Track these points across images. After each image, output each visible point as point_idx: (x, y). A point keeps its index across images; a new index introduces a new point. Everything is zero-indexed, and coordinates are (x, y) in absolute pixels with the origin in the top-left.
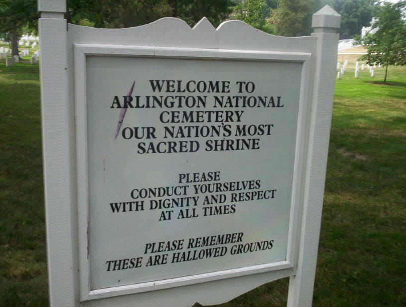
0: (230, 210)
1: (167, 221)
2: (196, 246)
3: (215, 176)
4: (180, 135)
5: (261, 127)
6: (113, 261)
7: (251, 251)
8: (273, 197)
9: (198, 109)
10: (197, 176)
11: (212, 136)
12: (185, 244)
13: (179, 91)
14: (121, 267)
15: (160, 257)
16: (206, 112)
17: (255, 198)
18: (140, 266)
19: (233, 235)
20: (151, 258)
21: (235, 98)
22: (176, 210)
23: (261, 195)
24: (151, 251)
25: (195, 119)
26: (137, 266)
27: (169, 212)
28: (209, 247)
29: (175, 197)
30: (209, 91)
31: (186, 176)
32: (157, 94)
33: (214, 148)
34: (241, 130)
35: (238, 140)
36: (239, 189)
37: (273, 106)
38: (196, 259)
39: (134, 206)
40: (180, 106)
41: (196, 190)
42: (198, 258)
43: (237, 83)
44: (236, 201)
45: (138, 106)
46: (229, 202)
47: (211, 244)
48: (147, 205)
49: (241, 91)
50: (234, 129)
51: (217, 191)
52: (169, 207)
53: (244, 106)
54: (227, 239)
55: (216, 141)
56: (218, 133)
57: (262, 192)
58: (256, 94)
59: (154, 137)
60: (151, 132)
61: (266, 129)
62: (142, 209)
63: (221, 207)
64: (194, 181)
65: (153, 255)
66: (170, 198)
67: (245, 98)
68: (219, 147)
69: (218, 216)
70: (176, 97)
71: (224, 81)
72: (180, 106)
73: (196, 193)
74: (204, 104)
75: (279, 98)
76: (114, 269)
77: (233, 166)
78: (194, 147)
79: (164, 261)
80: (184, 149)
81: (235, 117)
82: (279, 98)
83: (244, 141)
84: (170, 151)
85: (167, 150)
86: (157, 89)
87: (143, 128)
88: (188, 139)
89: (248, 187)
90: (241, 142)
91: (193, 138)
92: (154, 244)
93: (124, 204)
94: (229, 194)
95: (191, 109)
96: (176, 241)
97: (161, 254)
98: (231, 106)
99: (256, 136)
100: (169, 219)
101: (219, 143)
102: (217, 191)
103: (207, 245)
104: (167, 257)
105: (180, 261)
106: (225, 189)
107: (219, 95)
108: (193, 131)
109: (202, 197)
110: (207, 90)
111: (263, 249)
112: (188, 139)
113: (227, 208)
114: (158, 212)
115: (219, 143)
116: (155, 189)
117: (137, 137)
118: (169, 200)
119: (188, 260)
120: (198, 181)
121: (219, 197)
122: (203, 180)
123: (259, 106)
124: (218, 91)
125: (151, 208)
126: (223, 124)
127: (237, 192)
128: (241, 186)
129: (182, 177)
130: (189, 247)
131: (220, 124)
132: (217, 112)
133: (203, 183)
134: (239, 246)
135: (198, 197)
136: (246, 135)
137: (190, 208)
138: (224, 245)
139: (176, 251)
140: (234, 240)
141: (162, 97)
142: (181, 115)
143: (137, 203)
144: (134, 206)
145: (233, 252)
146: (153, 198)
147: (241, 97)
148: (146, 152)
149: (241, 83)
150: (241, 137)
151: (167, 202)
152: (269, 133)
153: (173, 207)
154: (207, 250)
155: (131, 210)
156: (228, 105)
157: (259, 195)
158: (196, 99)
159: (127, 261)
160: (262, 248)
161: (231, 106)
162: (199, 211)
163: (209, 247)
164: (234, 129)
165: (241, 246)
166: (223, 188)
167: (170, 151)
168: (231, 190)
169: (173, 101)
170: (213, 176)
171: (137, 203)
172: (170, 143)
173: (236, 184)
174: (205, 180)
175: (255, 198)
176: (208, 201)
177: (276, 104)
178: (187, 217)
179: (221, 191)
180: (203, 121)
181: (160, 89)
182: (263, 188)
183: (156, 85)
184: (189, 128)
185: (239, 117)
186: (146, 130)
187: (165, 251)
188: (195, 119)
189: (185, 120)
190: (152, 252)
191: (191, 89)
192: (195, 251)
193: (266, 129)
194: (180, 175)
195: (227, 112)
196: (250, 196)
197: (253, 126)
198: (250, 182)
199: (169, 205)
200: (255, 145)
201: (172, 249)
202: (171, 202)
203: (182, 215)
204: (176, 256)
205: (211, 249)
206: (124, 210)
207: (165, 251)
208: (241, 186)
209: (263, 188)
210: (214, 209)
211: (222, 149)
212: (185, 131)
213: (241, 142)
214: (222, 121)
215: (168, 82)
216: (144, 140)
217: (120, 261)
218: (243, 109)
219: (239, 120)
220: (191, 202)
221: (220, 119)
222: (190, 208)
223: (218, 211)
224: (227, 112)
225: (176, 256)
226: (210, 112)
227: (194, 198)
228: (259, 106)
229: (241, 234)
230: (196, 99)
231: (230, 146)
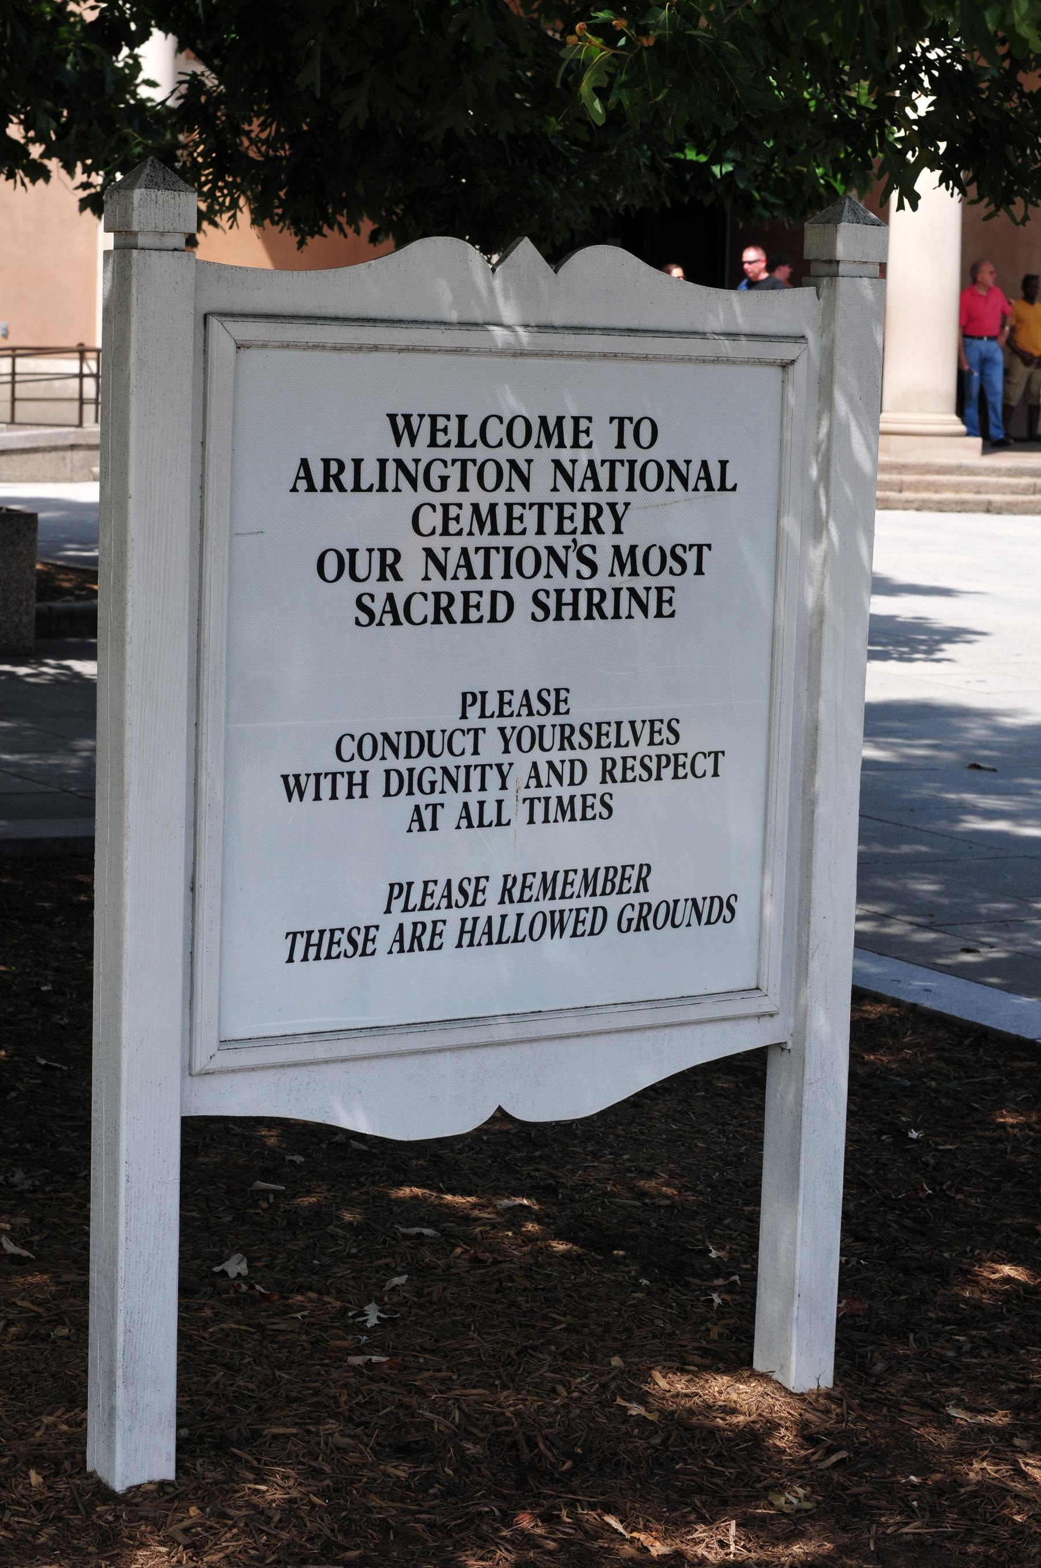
0: (599, 808)
1: (428, 834)
2: (521, 900)
3: (556, 700)
4: (463, 573)
5: (679, 551)
6: (302, 933)
7: (674, 925)
8: (716, 774)
9: (511, 498)
10: (507, 697)
11: (548, 576)
12: (493, 890)
13: (461, 444)
14: (323, 953)
15: (424, 925)
16: (531, 505)
17: (668, 773)
18: (373, 954)
19: (624, 868)
20: (401, 927)
21: (482, 552)
22: (453, 801)
23: (684, 766)
24: (402, 907)
25: (502, 526)
26: (364, 954)
27: (435, 806)
28: (558, 905)
29: (448, 761)
30: (538, 446)
31: (479, 697)
32: (406, 452)
33: (553, 614)
34: (626, 560)
35: (617, 591)
36: (623, 742)
37: (470, 825)
38: (523, 940)
39: (342, 783)
40: (463, 488)
41: (506, 742)
42: (528, 938)
43: (612, 419)
44: (614, 781)
45: (357, 488)
46: (593, 784)
47: (563, 897)
48: (376, 784)
49: (621, 445)
50: (604, 559)
51: (562, 748)
52: (433, 791)
53: (631, 488)
54: (606, 880)
55: (559, 592)
56: (563, 568)
57: (686, 755)
58: (661, 453)
59: (397, 577)
60: (389, 565)
61: (690, 557)
62: (364, 795)
63: (572, 798)
64: (501, 715)
65: (408, 919)
66: (437, 763)
67: (632, 463)
68: (567, 612)
69: (565, 826)
70: (454, 461)
71: (576, 415)
72: (463, 488)
73: (506, 751)
74: (526, 482)
75: (723, 464)
76: (305, 959)
77: (609, 669)
78: (500, 610)
79: (437, 942)
80: (474, 614)
81: (607, 521)
82: (723, 464)
83: (633, 592)
84: (437, 621)
85: (431, 618)
86: (406, 439)
87: (370, 551)
88: (486, 586)
89: (645, 738)
90: (625, 595)
91: (497, 583)
92: (410, 884)
93: (318, 776)
94: (593, 758)
95: (492, 497)
96: (469, 880)
97: (427, 917)
98: (597, 488)
99: (665, 579)
100: (434, 828)
101: (568, 597)
102: (562, 748)
103: (553, 898)
104: (488, 884)
105: (479, 944)
106: (585, 743)
107: (565, 455)
108: (497, 561)
109: (521, 764)
110: (533, 441)
111: (708, 922)
112: (486, 586)
113: (590, 800)
114: (404, 804)
115: (568, 597)
116: (398, 734)
117: (354, 577)
119: (500, 942)
120: (511, 715)
121: (567, 765)
122: (524, 711)
123: (670, 489)
124: (561, 445)
125: (387, 794)
126: (574, 541)
127: (617, 754)
128: (627, 735)
130: (502, 902)
131: (567, 540)
132: (561, 506)
133: (524, 720)
134: (642, 905)
135: (511, 765)
136: (904, 209)
137: (491, 795)
138: (598, 901)
139: (469, 912)
140: (626, 886)
141: (417, 461)
142: (467, 513)
143: (351, 774)
144: (342, 783)
145: (624, 927)
146: (392, 762)
147: (622, 462)
148: (377, 621)
149: (621, 420)
150: (624, 581)
151: (428, 776)
152: (699, 572)
153: (443, 792)
154: (552, 913)
155: (334, 797)
156: (589, 484)
157: (676, 766)
158: (506, 467)
159: (338, 935)
160: (704, 919)
161: (597, 488)
162: (516, 812)
163: (558, 905)
164: (604, 559)
165: (646, 907)
166: (577, 738)
167: (437, 621)
168: (599, 746)
169: (444, 472)
170: (551, 700)
171: (351, 774)
172: (437, 595)
173: (614, 726)
174: (530, 713)
175: (668, 773)
176: (537, 777)
177: (716, 483)
178: (481, 825)
179: (572, 748)
180: (523, 532)
181: (413, 440)
182: (688, 745)
183: (402, 428)
184: (487, 550)
185: (618, 520)
186: (376, 555)
187: (439, 908)
188: (502, 526)
189: (476, 529)
190: (405, 909)
191: (492, 438)
192: (519, 916)
193: (690, 557)
194: (464, 695)
195: (587, 506)
196: (653, 766)
198: (652, 722)
199: (433, 784)
200: (662, 606)
201: (457, 906)
202: (439, 775)
203: (468, 817)
204: (468, 927)
205: (562, 912)
206: (317, 798)
207: (439, 908)
208: (627, 735)
209: (688, 745)
210: (553, 803)
211: (575, 617)
212: (477, 561)
213: (625, 595)
214: (574, 532)
215: (434, 418)
216: (372, 586)
217: (322, 932)
218: (630, 496)
219: (618, 530)
220: (493, 778)
221: (568, 526)
222: (491, 795)
223: (566, 809)
224: (587, 506)
225: (468, 927)
226: (541, 506)
227: (499, 766)
228: (670, 489)
229: (645, 869)
230: (506, 467)
231: (595, 610)
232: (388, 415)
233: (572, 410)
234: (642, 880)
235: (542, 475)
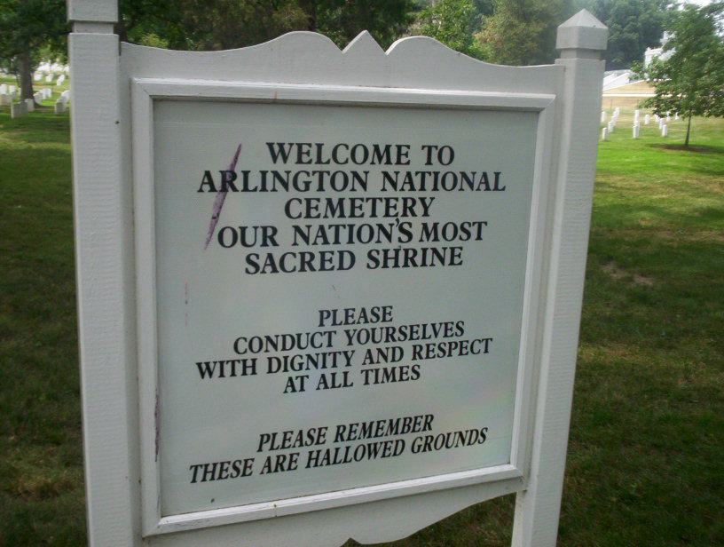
0: (411, 373)
1: (298, 394)
2: (349, 439)
3: (384, 313)
4: (320, 240)
5: (466, 226)
6: (201, 466)
7: (447, 447)
8: (486, 351)
9: (353, 195)
10: (350, 313)
11: (379, 242)
12: (331, 435)
13: (319, 161)
14: (217, 476)
15: (285, 457)
16: (368, 199)
17: (456, 352)
18: (250, 474)
19: (416, 418)
20: (269, 459)
21: (420, 175)
22: (314, 374)
23: (466, 347)
24: (269, 447)
25: (347, 212)
26: (244, 475)
27: (302, 378)
28: (373, 440)
29: (311, 351)
30: (373, 163)
31: (332, 313)
32: (280, 167)
33: (381, 264)
34: (430, 232)
35: (424, 250)
36: (427, 336)
38: (350, 461)
39: (239, 367)
40: (321, 189)
41: (350, 338)
42: (353, 460)
43: (423, 147)
44: (421, 358)
45: (246, 189)
46: (408, 360)
47: (376, 435)
48: (262, 365)
49: (429, 163)
50: (417, 231)
51: (387, 341)
52: (301, 368)
53: (435, 189)
54: (404, 425)
55: (386, 252)
56: (389, 237)
57: (467, 342)
58: (456, 167)
59: (275, 244)
60: (269, 236)
61: (474, 230)
62: (254, 373)
63: (393, 369)
64: (347, 323)
65: (273, 455)
66: (303, 353)
67: (436, 174)
68: (391, 263)
69: (389, 385)
70: (314, 173)
71: (399, 144)
72: (321, 189)
73: (350, 344)
74: (364, 185)
75: (497, 175)
76: (204, 480)
77: (416, 296)
78: (346, 262)
79: (293, 465)
80: (328, 265)
81: (419, 209)
82: (497, 175)
83: (435, 251)
84: (303, 269)
85: (298, 268)
86: (280, 159)
87: (256, 228)
88: (336, 248)
89: (442, 333)
90: (429, 253)
91: (344, 246)
92: (274, 435)
93: (222, 363)
94: (408, 346)
95: (341, 195)
96: (315, 430)
97: (287, 452)
98: (412, 189)
99: (457, 243)
100: (302, 389)
101: (391, 254)
102: (387, 341)
103: (370, 436)
104: (299, 458)
105: (321, 465)
106: (402, 337)
107: (391, 170)
108: (344, 234)
109: (360, 351)
110: (370, 160)
111: (469, 444)
112: (336, 248)
113: (405, 370)
114: (282, 378)
115: (391, 254)
116: (277, 336)
117: (244, 243)
118: (301, 357)
119: (335, 462)
120: (353, 323)
121: (391, 350)
122: (362, 320)
123: (461, 189)
124: (388, 162)
125: (270, 371)
126: (397, 220)
127: (423, 343)
128: (429, 331)
129: (325, 315)
130: (336, 441)
131: (392, 220)
132: (388, 200)
133: (362, 326)
134: (427, 437)
135: (353, 352)
137: (340, 370)
138: (399, 437)
139: (314, 448)
140: (417, 428)
141: (288, 172)
142: (323, 205)
143: (245, 361)
144: (239, 367)
145: (416, 450)
146: (272, 353)
147: (430, 173)
148: (261, 270)
149: (430, 148)
150: (429, 244)
151: (297, 360)
152: (479, 238)
153: (308, 369)
154: (369, 445)
155: (233, 374)
156: (407, 187)
157: (461, 348)
158: (350, 176)
159: (226, 466)
160: (467, 441)
161: (412, 189)
162: (356, 376)
163: (373, 440)
164: (417, 231)
165: (430, 439)
166: (397, 335)
167: (303, 269)
168: (411, 338)
169: (308, 179)
170: (380, 313)
171: (245, 361)
172: (303, 255)
173: (421, 327)
174: (366, 322)
175: (456, 352)
176: (371, 358)
177: (492, 186)
178: (333, 386)
179: (394, 340)
180: (362, 216)
181: (285, 159)
182: (469, 335)
183: (277, 151)
184: (337, 227)
185: (426, 208)
186: (260, 231)
187: (294, 446)
188: (347, 212)
189: (329, 213)
190: (272, 448)
191: (341, 158)
192: (348, 448)
193: (474, 230)
194: (322, 312)
195: (405, 200)
196: (447, 349)
197: (452, 225)
198: (446, 324)
199: (301, 365)
200: (454, 258)
201: (306, 444)
202: (305, 360)
203: (325, 382)
204: (314, 455)
205: (375, 444)
206: (222, 375)
207: (294, 446)
208: (429, 331)
209: (469, 335)
210: (381, 373)
211: (396, 265)
212: (330, 234)
213: (429, 253)
214: (397, 215)
215: (300, 146)
216: (257, 249)
217: (215, 465)
218: (434, 194)
219: (426, 214)
220: (341, 360)
221: (392, 212)
222: (340, 370)
223: (389, 375)
224: (405, 200)
225: (314, 455)
226: (374, 200)
227: (346, 353)
228: (461, 189)
229: (430, 418)
230: (350, 176)
231: (410, 261)
232: (221, 172)
233: (394, 143)
234: (428, 425)
235: (375, 186)
